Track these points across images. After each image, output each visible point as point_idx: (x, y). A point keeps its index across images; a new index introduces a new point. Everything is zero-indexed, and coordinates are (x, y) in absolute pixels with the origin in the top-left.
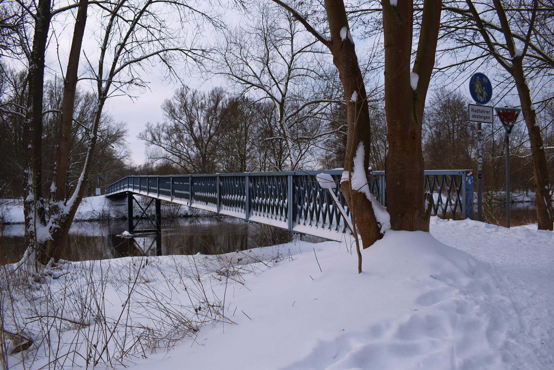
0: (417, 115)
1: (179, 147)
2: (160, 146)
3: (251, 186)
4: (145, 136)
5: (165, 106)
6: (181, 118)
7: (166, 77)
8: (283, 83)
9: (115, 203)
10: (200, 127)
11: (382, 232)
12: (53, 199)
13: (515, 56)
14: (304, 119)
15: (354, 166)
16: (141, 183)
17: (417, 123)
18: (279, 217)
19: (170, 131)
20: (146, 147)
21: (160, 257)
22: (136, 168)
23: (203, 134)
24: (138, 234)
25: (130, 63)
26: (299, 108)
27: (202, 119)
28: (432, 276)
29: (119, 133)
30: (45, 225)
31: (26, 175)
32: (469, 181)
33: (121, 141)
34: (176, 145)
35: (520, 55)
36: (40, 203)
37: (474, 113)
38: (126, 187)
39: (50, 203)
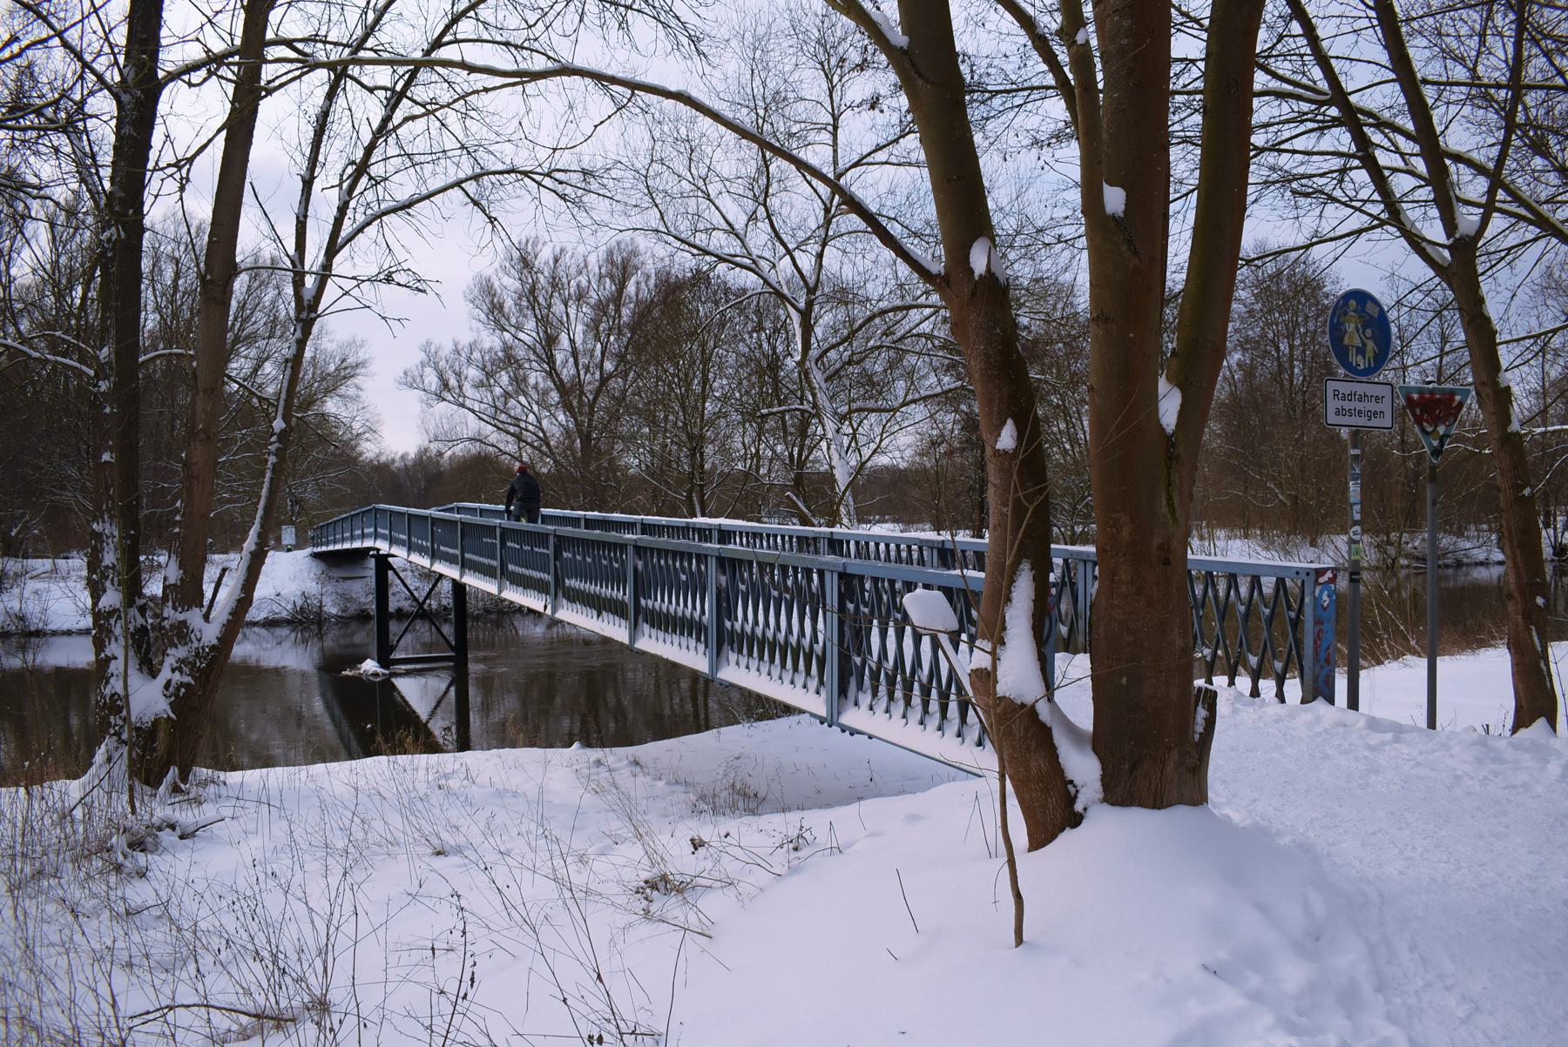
0: (1176, 499)
1: (515, 407)
2: (462, 405)
3: (724, 584)
4: (418, 380)
5: (476, 292)
6: (519, 328)
7: (482, 245)
8: (809, 248)
9: (336, 573)
10: (575, 354)
11: (1078, 807)
12: (174, 603)
13: (1457, 236)
14: (866, 357)
15: (1004, 629)
16: (412, 531)
17: (1175, 520)
18: (800, 679)
19: (489, 365)
20: (423, 411)
21: (471, 758)
22: (393, 461)
23: (582, 373)
24: (403, 667)
25: (379, 216)
26: (857, 325)
27: (580, 328)
28: (1205, 967)
29: (345, 368)
30: (154, 674)
31: (98, 536)
32: (1325, 597)
33: (352, 392)
34: (506, 403)
35: (1472, 233)
36: (138, 615)
37: (1339, 404)
38: (369, 536)
39: (165, 615)
